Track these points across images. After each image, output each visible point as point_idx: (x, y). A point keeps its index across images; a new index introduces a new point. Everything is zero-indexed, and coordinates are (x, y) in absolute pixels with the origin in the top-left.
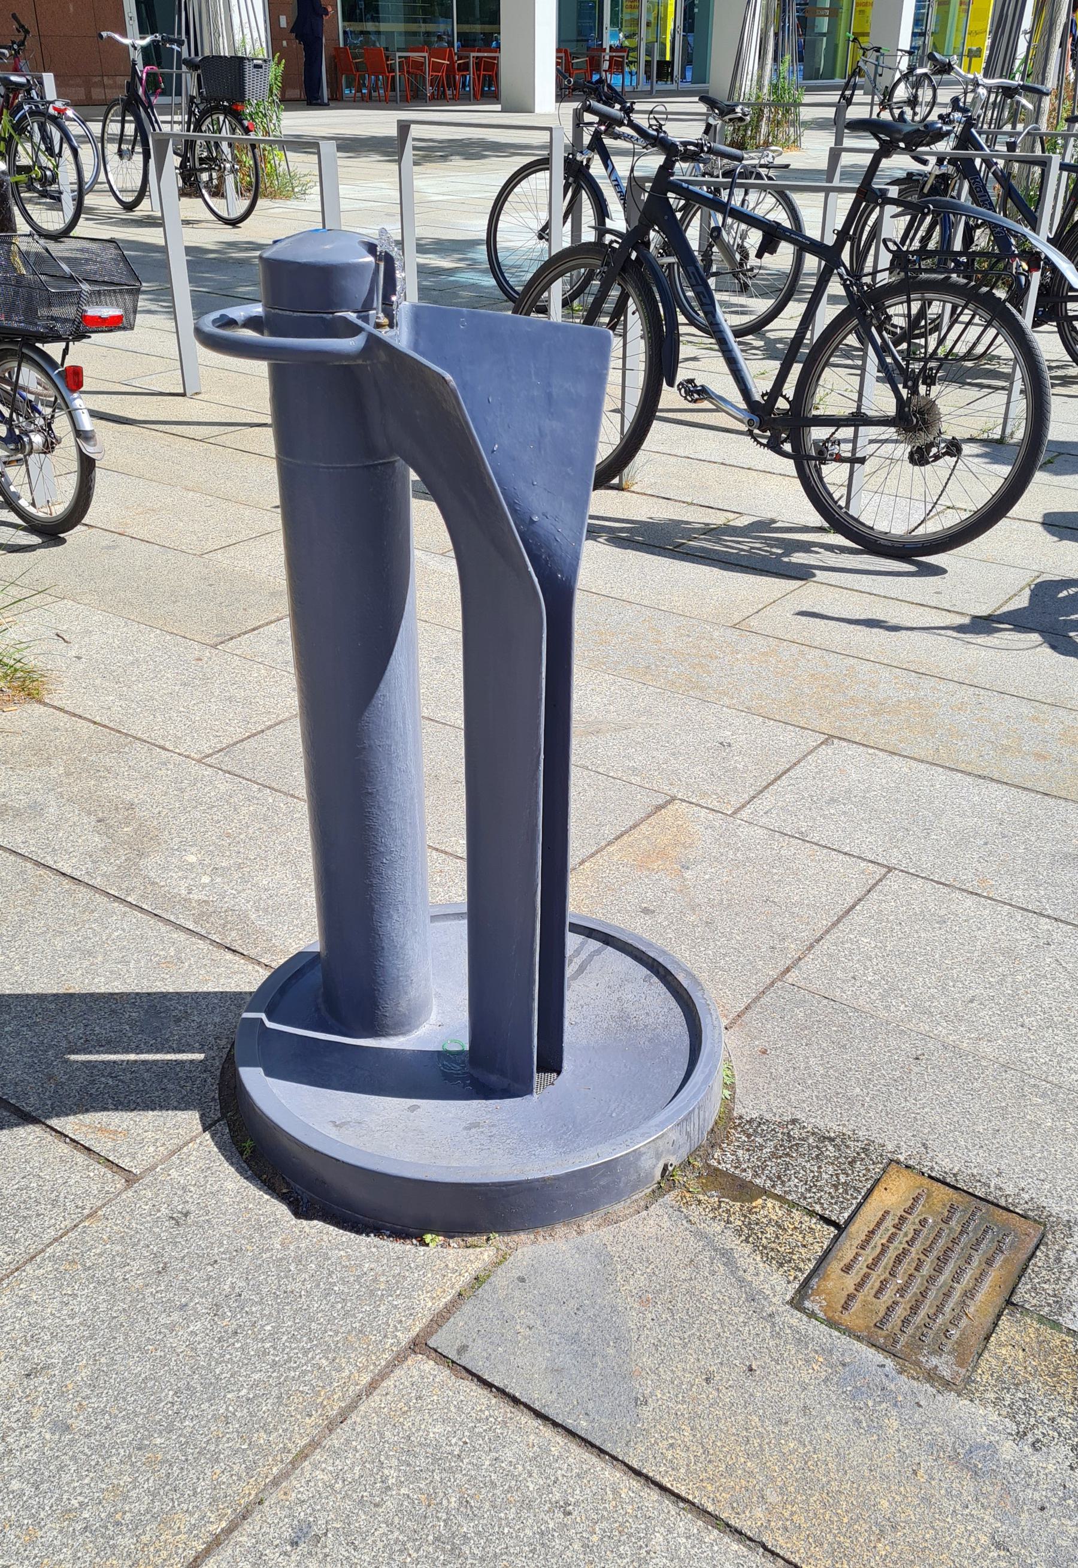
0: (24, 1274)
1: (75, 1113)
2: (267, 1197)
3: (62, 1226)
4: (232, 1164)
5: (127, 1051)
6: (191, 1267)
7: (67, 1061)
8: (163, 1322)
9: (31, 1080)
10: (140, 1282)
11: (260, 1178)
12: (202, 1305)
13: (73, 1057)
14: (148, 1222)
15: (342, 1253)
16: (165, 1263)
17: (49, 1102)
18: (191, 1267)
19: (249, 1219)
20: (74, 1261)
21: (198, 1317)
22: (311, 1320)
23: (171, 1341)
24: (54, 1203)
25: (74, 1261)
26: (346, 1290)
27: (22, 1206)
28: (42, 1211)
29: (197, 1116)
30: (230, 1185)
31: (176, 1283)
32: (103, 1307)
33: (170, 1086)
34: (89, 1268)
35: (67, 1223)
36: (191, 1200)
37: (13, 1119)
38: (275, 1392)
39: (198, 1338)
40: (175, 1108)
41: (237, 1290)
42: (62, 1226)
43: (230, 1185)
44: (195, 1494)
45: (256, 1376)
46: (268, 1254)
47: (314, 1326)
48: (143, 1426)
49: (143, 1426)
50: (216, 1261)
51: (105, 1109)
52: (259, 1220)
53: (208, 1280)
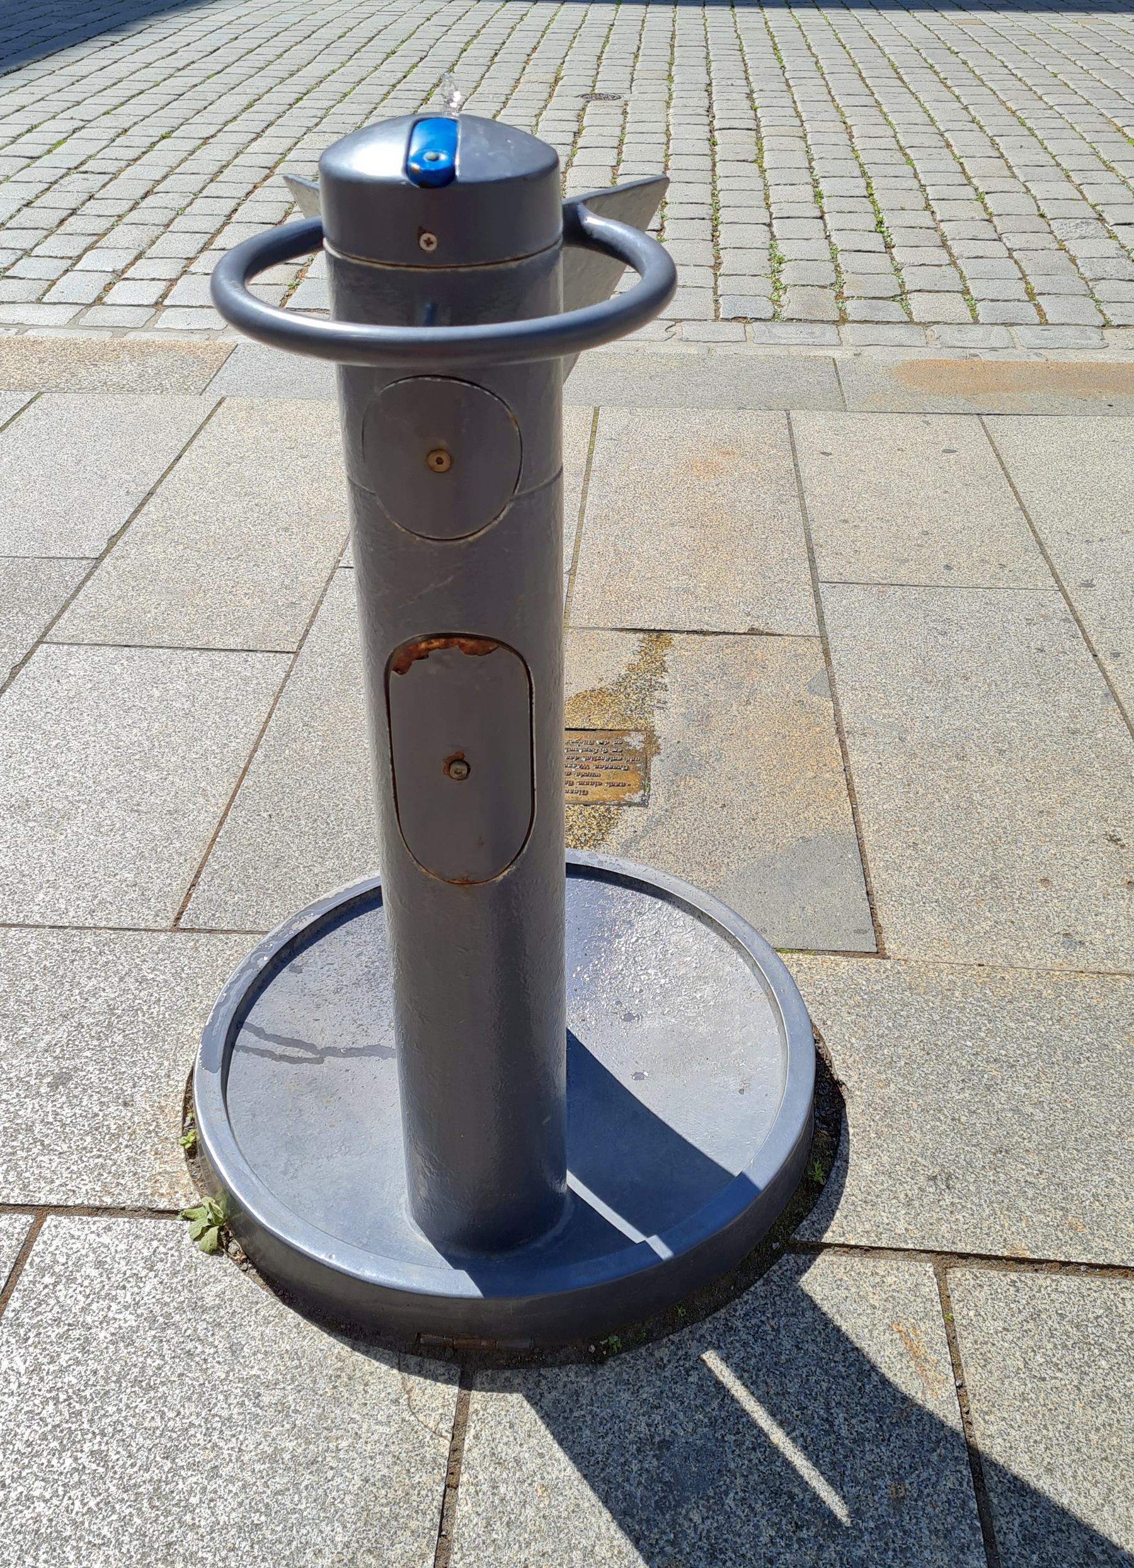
0: (1125, 1257)
1: (920, 1408)
2: (851, 1130)
3: (1048, 1282)
4: (842, 1186)
5: (775, 1452)
6: (977, 1133)
7: (855, 1513)
8: (1042, 1115)
9: (924, 1522)
10: (1031, 1158)
11: (836, 1148)
12: (999, 1099)
13: (840, 1510)
14: (973, 1203)
15: (853, 1040)
16: (995, 1154)
17: (934, 1457)
18: (977, 1133)
19: (889, 1126)
20: (1071, 1227)
21: (1011, 1095)
22: (934, 1023)
23: (1047, 1096)
24: (1035, 1316)
25: (1071, 1227)
26: (885, 1017)
27: (1069, 1344)
28: (1055, 1317)
29: (806, 1277)
30: (867, 1168)
31: (1002, 1132)
32: (1079, 1166)
33: (787, 1344)
34: (1062, 1209)
35: (1041, 1282)
36: (915, 1187)
37: (992, 1480)
38: (1009, 1007)
39: (1027, 1080)
40: (815, 1307)
41: (961, 1085)
42: (1048, 1282)
43: (867, 1168)
44: (1121, 1003)
45: (1012, 1025)
46: (907, 1088)
47: (936, 1017)
48: (1121, 1063)
49: (1121, 1063)
50: (953, 1119)
51: (885, 1382)
52: (881, 1119)
53: (974, 1112)
